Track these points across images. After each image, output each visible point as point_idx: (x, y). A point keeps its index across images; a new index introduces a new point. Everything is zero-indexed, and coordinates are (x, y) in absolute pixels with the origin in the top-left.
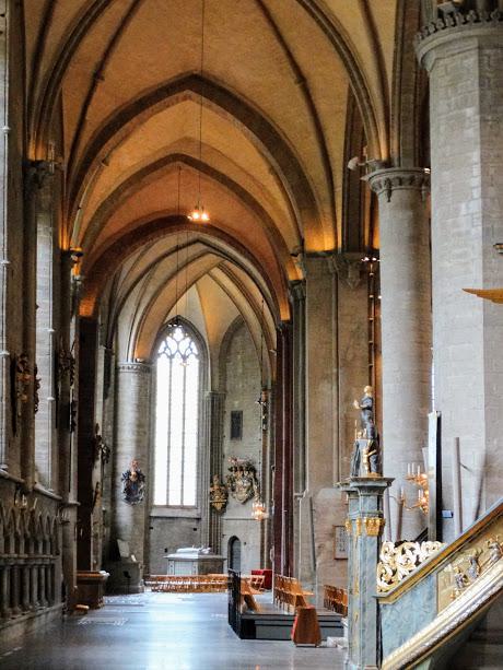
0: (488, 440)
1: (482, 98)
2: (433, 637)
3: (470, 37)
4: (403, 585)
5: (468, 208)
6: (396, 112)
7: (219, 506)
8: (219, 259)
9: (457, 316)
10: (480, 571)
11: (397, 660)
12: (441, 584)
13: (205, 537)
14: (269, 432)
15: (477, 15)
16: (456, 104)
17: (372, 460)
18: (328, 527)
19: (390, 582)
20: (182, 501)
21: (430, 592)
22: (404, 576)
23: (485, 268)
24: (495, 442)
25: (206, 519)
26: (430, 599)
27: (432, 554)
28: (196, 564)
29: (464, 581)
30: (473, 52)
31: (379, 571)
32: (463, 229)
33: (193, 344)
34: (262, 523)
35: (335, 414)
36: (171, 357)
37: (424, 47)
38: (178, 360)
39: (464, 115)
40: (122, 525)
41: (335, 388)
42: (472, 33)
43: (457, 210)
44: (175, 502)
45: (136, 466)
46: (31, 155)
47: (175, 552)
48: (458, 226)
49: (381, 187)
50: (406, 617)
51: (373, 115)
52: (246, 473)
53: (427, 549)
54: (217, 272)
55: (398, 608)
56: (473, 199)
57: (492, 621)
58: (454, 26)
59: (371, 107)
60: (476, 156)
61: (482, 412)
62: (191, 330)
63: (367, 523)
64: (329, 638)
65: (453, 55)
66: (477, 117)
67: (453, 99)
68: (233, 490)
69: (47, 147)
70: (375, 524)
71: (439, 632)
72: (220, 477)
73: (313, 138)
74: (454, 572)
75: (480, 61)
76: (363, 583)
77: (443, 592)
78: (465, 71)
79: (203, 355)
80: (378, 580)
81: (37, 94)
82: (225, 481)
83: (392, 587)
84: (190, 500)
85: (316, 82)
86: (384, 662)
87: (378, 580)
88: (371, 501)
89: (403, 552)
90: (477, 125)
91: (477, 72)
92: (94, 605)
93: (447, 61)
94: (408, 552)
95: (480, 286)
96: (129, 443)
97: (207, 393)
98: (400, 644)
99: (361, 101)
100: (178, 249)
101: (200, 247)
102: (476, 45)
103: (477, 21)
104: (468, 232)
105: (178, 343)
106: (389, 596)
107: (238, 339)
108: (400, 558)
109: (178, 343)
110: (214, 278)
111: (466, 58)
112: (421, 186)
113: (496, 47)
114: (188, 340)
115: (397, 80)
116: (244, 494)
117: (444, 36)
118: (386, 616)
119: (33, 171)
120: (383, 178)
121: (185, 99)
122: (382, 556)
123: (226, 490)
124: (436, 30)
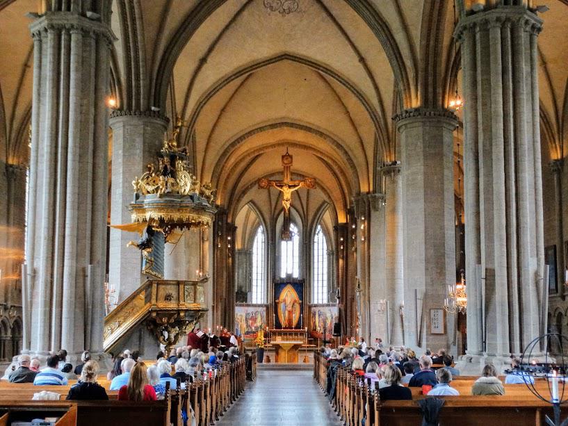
23: (123, 216)
46: (10, 162)
69: (19, 158)
75: (124, 131)
81: (13, 135)
113: (131, 125)
119: (11, 169)
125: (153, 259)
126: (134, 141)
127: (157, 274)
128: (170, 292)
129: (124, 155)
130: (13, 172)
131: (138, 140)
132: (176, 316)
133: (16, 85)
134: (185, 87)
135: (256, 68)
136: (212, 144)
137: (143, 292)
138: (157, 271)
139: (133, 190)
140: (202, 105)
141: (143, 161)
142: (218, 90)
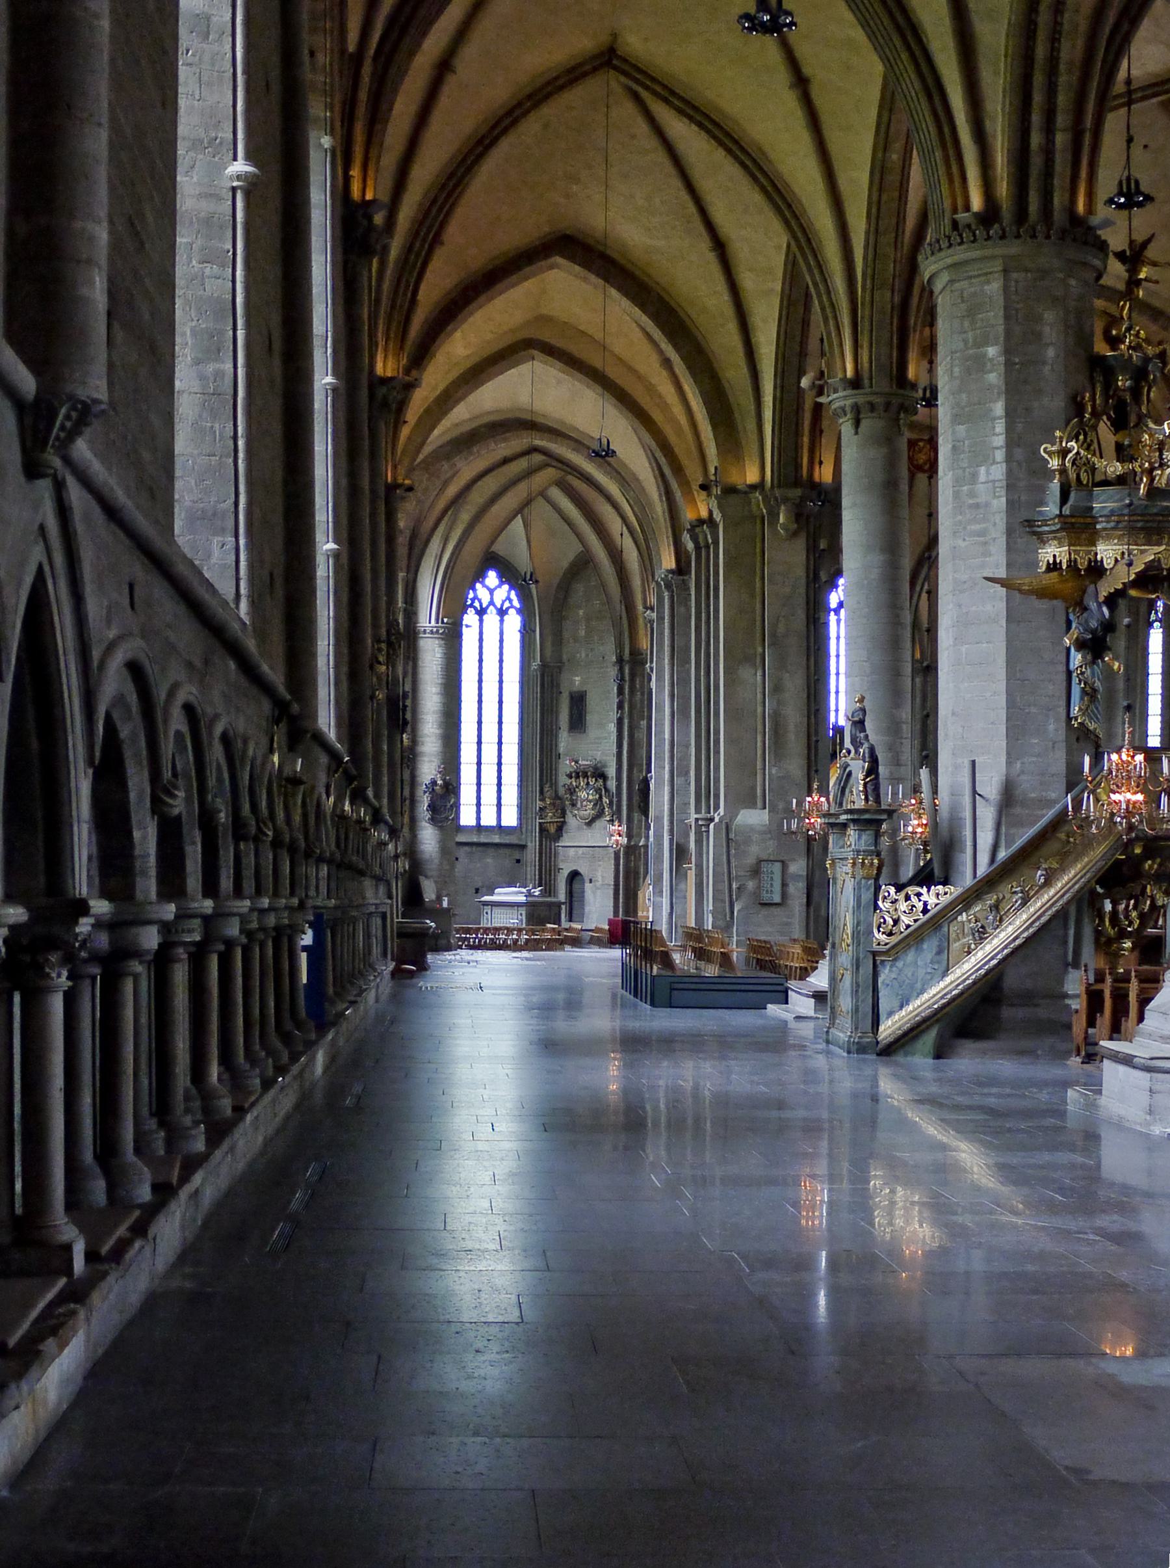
0: (1009, 763)
1: (1008, 334)
2: (942, 998)
3: (993, 257)
4: (907, 937)
5: (988, 473)
6: (867, 313)
7: (552, 829)
8: (559, 474)
9: (974, 608)
10: (1001, 920)
11: (897, 1025)
12: (953, 936)
13: (531, 869)
14: (626, 721)
15: (1004, 230)
16: (975, 340)
17: (870, 787)
18: (750, 860)
19: (890, 934)
20: (478, 818)
21: (939, 946)
22: (908, 926)
23: (1009, 549)
24: (1019, 765)
25: (533, 845)
26: (939, 953)
27: (944, 900)
28: (523, 911)
29: (981, 935)
30: (996, 275)
31: (876, 920)
32: (982, 499)
33: (513, 593)
34: (617, 855)
35: (759, 709)
36: (481, 612)
37: (929, 266)
38: (491, 618)
39: (985, 355)
40: (426, 856)
41: (759, 673)
42: (998, 251)
43: (974, 476)
44: (488, 819)
45: (444, 773)
47: (492, 894)
48: (976, 497)
49: (845, 415)
50: (910, 974)
51: (835, 318)
52: (592, 782)
53: (938, 895)
54: (556, 493)
55: (900, 964)
56: (994, 462)
57: (1011, 981)
58: (973, 242)
59: (832, 305)
60: (999, 408)
61: (1003, 729)
62: (509, 574)
63: (863, 863)
64: (769, 1006)
65: (970, 277)
66: (1002, 359)
67: (970, 334)
68: (574, 805)
70: (872, 864)
71: (951, 991)
72: (554, 784)
73: (732, 327)
74: (969, 921)
75: (1006, 288)
76: (856, 934)
77: (955, 946)
78: (987, 300)
79: (526, 612)
80: (875, 931)
81: (386, 285)
82: (561, 791)
83: (894, 940)
84: (510, 818)
85: (741, 252)
86: (881, 1028)
87: (875, 931)
88: (867, 837)
89: (908, 898)
90: (1002, 368)
91: (1001, 302)
92: (423, 967)
93: (964, 284)
94: (914, 899)
95: (1002, 573)
96: (433, 739)
97: (536, 664)
98: (901, 1007)
99: (819, 296)
100: (506, 461)
101: (538, 458)
102: (1000, 268)
103: (1003, 237)
104: (987, 505)
105: (491, 591)
106: (889, 950)
107: (579, 589)
108: (903, 906)
109: (491, 591)
110: (549, 501)
111: (988, 282)
112: (899, 413)
114: (506, 587)
115: (869, 271)
116: (589, 811)
117: (960, 254)
118: (885, 975)
119: (383, 390)
120: (849, 402)
121: (551, 267)
122: (880, 903)
123: (561, 805)
124: (950, 246)
129: (1008, 364)
131: (1049, 316)
135: (909, 48)
139: (1048, 474)
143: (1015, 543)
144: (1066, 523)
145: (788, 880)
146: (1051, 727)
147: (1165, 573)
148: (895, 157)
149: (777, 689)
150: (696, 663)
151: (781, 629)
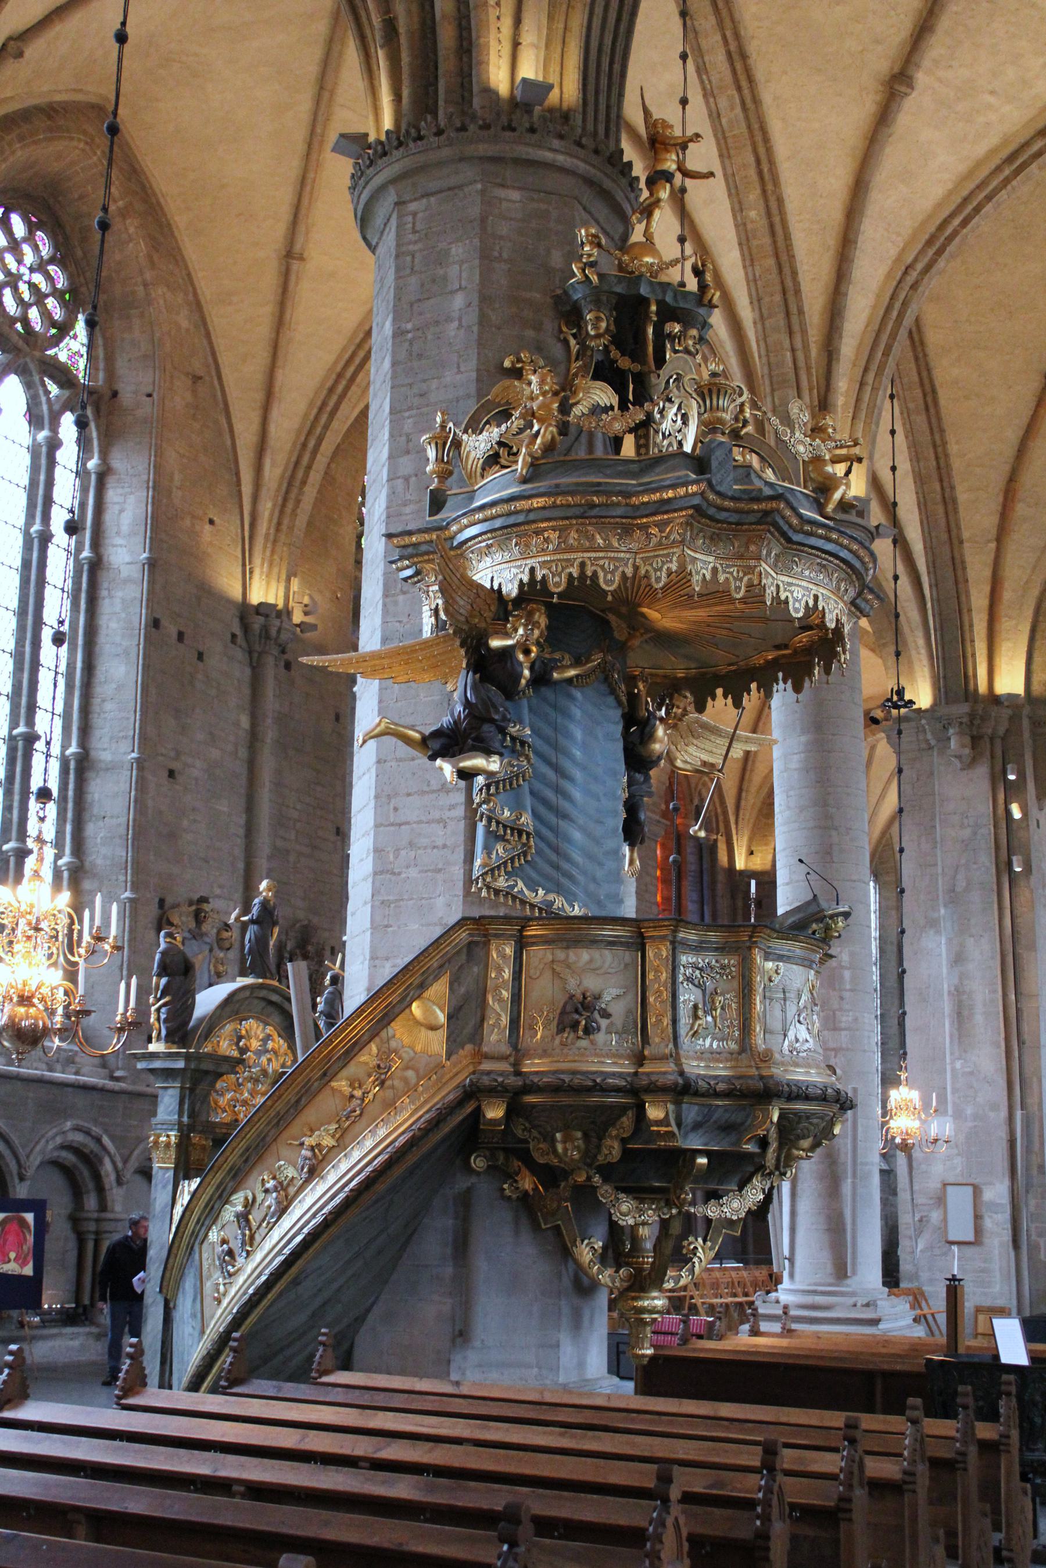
46: (256, 597)
125: (526, 820)
126: (441, 259)
127: (559, 902)
128: (592, 983)
130: (265, 629)
132: (627, 1121)
133: (264, 330)
134: (834, 212)
136: (1021, 509)
137: (440, 988)
138: (559, 889)
140: (914, 275)
141: (481, 344)
142: (977, 210)
143: (396, 603)
144: (404, 547)
145: (984, 1211)
146: (440, 902)
147: (610, 598)
148: (753, 214)
149: (958, 959)
150: (109, 917)
151: (960, 885)
